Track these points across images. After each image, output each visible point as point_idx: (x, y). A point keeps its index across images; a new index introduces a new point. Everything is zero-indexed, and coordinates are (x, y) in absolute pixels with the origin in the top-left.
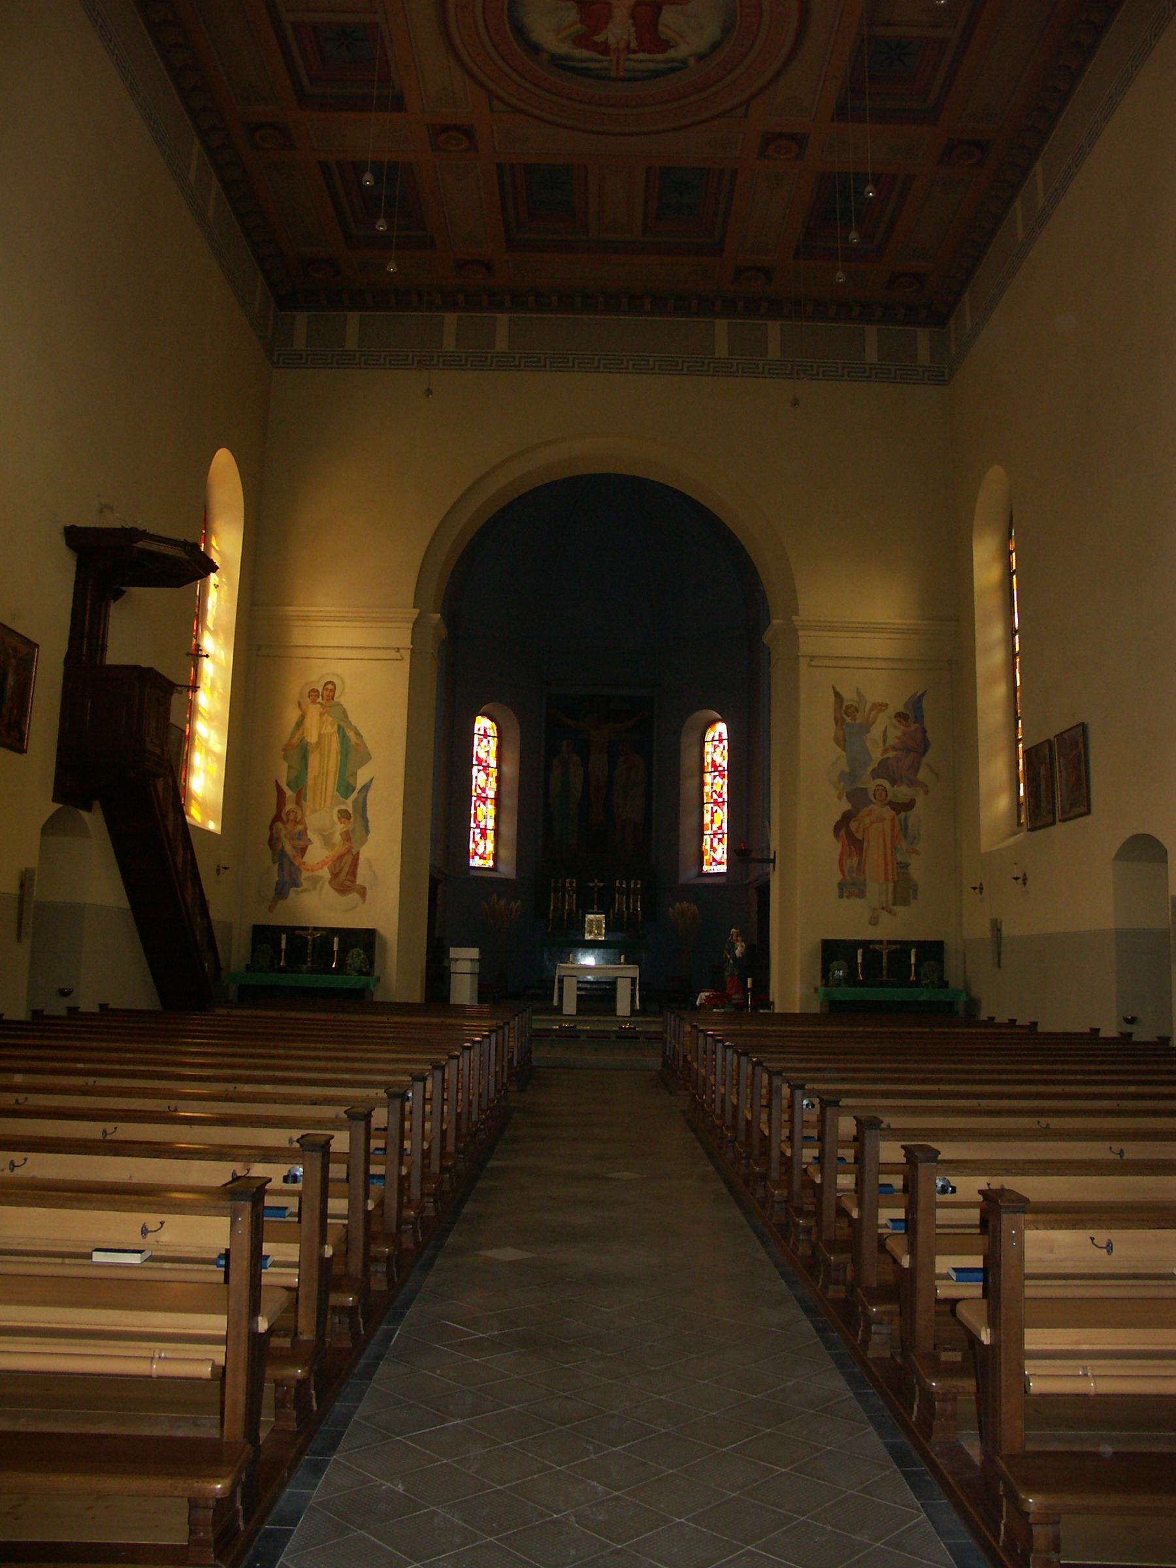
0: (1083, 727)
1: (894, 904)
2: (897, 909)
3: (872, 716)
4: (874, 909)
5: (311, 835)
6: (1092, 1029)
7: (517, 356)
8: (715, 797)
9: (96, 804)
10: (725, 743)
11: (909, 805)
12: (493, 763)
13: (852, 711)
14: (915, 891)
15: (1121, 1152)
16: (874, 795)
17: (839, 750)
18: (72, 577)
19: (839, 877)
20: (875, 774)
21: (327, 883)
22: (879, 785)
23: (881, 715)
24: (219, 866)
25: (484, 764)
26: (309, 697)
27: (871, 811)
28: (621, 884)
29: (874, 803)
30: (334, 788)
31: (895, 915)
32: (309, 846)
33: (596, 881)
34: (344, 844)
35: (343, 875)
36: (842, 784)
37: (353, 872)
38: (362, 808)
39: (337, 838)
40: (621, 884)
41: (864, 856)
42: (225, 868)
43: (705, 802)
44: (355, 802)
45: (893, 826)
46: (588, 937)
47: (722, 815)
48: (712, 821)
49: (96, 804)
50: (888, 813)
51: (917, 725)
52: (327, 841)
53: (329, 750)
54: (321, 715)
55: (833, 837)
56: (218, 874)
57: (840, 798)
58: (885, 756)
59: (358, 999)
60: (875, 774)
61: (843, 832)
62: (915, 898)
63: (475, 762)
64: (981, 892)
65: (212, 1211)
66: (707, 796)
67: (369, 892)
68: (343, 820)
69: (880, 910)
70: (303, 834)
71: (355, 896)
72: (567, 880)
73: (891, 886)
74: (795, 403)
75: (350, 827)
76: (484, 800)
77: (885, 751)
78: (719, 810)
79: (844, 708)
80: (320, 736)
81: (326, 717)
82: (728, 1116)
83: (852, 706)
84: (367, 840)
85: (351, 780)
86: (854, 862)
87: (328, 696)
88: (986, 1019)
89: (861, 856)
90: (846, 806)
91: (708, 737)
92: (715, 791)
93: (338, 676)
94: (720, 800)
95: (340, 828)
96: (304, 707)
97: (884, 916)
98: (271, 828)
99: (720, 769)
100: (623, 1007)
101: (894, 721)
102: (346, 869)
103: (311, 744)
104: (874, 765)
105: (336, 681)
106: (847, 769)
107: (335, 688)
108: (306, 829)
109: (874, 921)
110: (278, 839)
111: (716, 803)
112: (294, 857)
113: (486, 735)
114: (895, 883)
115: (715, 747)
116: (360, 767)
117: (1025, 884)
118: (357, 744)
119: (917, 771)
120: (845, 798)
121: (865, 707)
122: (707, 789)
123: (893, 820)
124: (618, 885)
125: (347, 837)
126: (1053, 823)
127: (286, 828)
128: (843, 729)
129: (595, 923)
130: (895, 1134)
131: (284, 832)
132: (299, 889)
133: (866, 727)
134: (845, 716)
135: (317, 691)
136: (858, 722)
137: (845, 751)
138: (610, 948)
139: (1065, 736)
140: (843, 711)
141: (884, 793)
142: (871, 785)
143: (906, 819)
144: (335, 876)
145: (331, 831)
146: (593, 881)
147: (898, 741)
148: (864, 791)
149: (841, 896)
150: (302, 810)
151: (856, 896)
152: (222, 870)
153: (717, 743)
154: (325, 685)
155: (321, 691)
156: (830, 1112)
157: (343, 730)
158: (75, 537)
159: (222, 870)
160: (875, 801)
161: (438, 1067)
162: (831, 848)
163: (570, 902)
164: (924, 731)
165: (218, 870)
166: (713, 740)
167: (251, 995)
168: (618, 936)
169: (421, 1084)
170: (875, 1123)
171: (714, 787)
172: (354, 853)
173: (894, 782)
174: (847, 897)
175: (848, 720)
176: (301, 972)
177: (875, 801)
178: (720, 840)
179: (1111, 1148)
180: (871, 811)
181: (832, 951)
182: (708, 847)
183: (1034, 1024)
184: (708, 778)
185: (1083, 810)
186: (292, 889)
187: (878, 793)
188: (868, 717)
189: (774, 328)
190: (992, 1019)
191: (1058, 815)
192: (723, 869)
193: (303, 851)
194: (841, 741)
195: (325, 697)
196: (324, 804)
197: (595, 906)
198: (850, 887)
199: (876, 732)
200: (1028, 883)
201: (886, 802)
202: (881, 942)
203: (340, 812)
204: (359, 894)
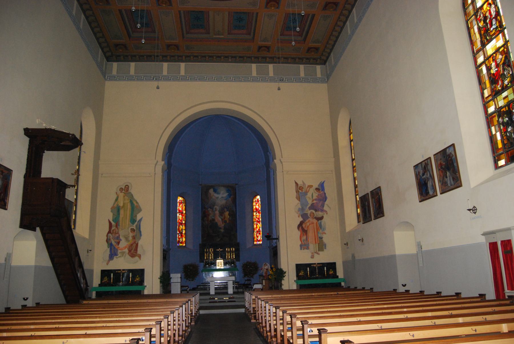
0: (379, 187)
1: (319, 251)
2: (320, 252)
3: (308, 190)
4: (312, 253)
5: (121, 237)
6: (363, 288)
7: (188, 77)
8: (257, 219)
9: (38, 229)
10: (260, 202)
11: (322, 218)
12: (184, 212)
13: (301, 188)
14: (325, 246)
15: (413, 336)
16: (310, 215)
17: (298, 202)
18: (27, 147)
19: (300, 243)
20: (310, 208)
21: (127, 254)
22: (311, 212)
23: (311, 189)
24: (88, 250)
25: (181, 212)
26: (120, 190)
27: (309, 220)
28: (228, 249)
29: (310, 218)
30: (129, 221)
31: (319, 254)
32: (121, 241)
33: (219, 249)
34: (133, 240)
35: (132, 251)
36: (299, 212)
37: (136, 250)
38: (139, 227)
39: (130, 238)
40: (228, 249)
41: (308, 235)
42: (90, 250)
43: (254, 221)
44: (136, 226)
45: (317, 225)
46: (218, 268)
47: (260, 225)
48: (257, 228)
49: (38, 229)
50: (315, 221)
51: (322, 192)
52: (127, 239)
53: (127, 208)
54: (124, 196)
55: (297, 229)
56: (88, 253)
57: (299, 217)
58: (313, 202)
59: (139, 294)
60: (310, 208)
61: (300, 228)
62: (325, 248)
63: (178, 212)
64: (347, 245)
65: (481, 92)
66: (254, 219)
67: (142, 256)
68: (132, 232)
69: (314, 253)
70: (118, 238)
71: (137, 258)
72: (210, 249)
73: (317, 245)
74: (279, 89)
75: (135, 234)
76: (181, 224)
77: (313, 201)
78: (258, 224)
79: (298, 187)
80: (124, 204)
81: (125, 197)
82: (273, 331)
83: (301, 186)
84: (141, 238)
85: (135, 218)
86: (305, 237)
87: (126, 190)
88: (362, 288)
89: (307, 235)
90: (301, 219)
91: (254, 201)
92: (257, 218)
93: (132, 186)
94: (259, 220)
95: (131, 235)
96: (118, 194)
97: (316, 255)
98: (107, 236)
99: (258, 210)
100: (230, 291)
101: (315, 191)
102: (134, 248)
103: (121, 206)
104: (309, 205)
105: (130, 185)
106: (301, 207)
107: (129, 187)
108: (119, 236)
109: (312, 257)
110: (110, 239)
111: (257, 221)
112: (115, 245)
113: (181, 203)
114: (319, 244)
115: (256, 203)
116: (137, 214)
117: (363, 242)
118: (137, 206)
119: (323, 207)
120: (300, 217)
121: (305, 187)
122: (255, 217)
123: (317, 223)
124: (227, 250)
125: (134, 237)
126: (371, 220)
127: (112, 236)
128: (298, 194)
129: (220, 263)
130: (312, 325)
131: (111, 237)
132: (117, 257)
133: (306, 193)
134: (299, 190)
135: (123, 188)
136: (303, 191)
137: (299, 201)
138: (225, 271)
139: (374, 191)
140: (298, 189)
141: (313, 215)
142: (309, 212)
143: (321, 223)
144: (130, 251)
145: (128, 236)
146: (219, 249)
147: (317, 197)
148: (307, 214)
149: (301, 249)
150: (118, 230)
151: (306, 249)
152: (89, 251)
153: (257, 202)
154: (125, 186)
155: (124, 188)
156: (251, 295)
157: (132, 202)
158: (28, 132)
159: (89, 251)
160: (310, 217)
161: (167, 317)
162: (297, 233)
163: (211, 257)
164: (325, 194)
165: (88, 251)
166: (255, 201)
167: (100, 295)
168: (228, 266)
169: (173, 314)
170: (325, 331)
171: (257, 216)
172: (136, 243)
173: (316, 211)
174: (303, 249)
175: (300, 191)
176: (119, 286)
177: (310, 217)
178: (260, 234)
179: (410, 334)
180: (309, 220)
181: (299, 267)
182: (255, 236)
183: (372, 289)
184: (255, 214)
185: (381, 215)
186: (115, 257)
187: (311, 215)
188: (307, 190)
189: (271, 66)
190: (356, 288)
191: (373, 217)
192: (261, 242)
193: (118, 243)
194: (298, 198)
195: (125, 190)
196: (126, 227)
197: (220, 257)
198: (304, 246)
199: (309, 195)
200: (364, 241)
201: (314, 217)
202: (315, 264)
203: (131, 229)
204: (138, 257)
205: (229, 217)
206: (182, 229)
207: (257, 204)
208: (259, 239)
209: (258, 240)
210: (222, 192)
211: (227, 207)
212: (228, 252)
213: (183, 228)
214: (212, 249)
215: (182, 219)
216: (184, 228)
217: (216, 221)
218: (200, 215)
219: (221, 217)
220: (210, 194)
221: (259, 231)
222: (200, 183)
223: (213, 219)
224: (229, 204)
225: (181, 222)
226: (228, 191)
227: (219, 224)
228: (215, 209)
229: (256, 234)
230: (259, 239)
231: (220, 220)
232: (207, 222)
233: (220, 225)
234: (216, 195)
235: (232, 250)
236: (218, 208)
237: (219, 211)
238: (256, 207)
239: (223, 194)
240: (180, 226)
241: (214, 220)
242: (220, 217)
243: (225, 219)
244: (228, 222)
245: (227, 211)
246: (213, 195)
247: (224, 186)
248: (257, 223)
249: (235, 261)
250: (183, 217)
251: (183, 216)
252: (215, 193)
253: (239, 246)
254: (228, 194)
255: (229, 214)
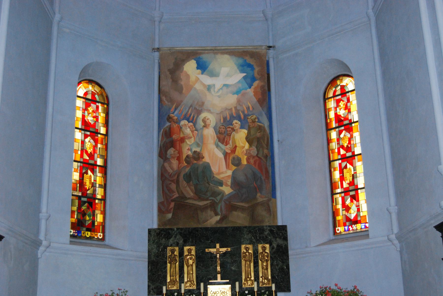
25: (91, 129)
33: (218, 246)
48: (342, 178)
72: (186, 248)
78: (349, 166)
99: (346, 122)
113: (94, 101)
115: (338, 102)
166: (334, 96)
171: (341, 142)
182: (339, 206)
197: (219, 276)
205: (247, 146)
206: (93, 185)
207: (342, 104)
208: (352, 217)
209: (348, 219)
210: (224, 70)
211: (242, 116)
212: (247, 258)
213: (95, 181)
214: (193, 248)
215: (94, 151)
216: (99, 179)
217: (207, 159)
218: (156, 141)
219: (223, 146)
220: (188, 76)
221: (351, 188)
222: (157, 46)
223: (195, 152)
224: (248, 108)
225: (91, 162)
226: (243, 67)
227: (215, 169)
228: (204, 121)
229: (340, 200)
230: (352, 217)
231: (221, 155)
232: (175, 163)
233: (219, 174)
234: (206, 80)
235: (260, 250)
236: (212, 120)
237: (215, 128)
238: (336, 114)
239: (228, 75)
240: (87, 173)
241: (198, 156)
242: (217, 146)
243: (237, 153)
244: (244, 162)
245: (242, 127)
246: (198, 79)
247: (232, 53)
248: (343, 164)
249: (274, 289)
250: (99, 146)
251: (96, 141)
252: (202, 73)
253: (285, 239)
254: (244, 78)
255: (249, 139)
